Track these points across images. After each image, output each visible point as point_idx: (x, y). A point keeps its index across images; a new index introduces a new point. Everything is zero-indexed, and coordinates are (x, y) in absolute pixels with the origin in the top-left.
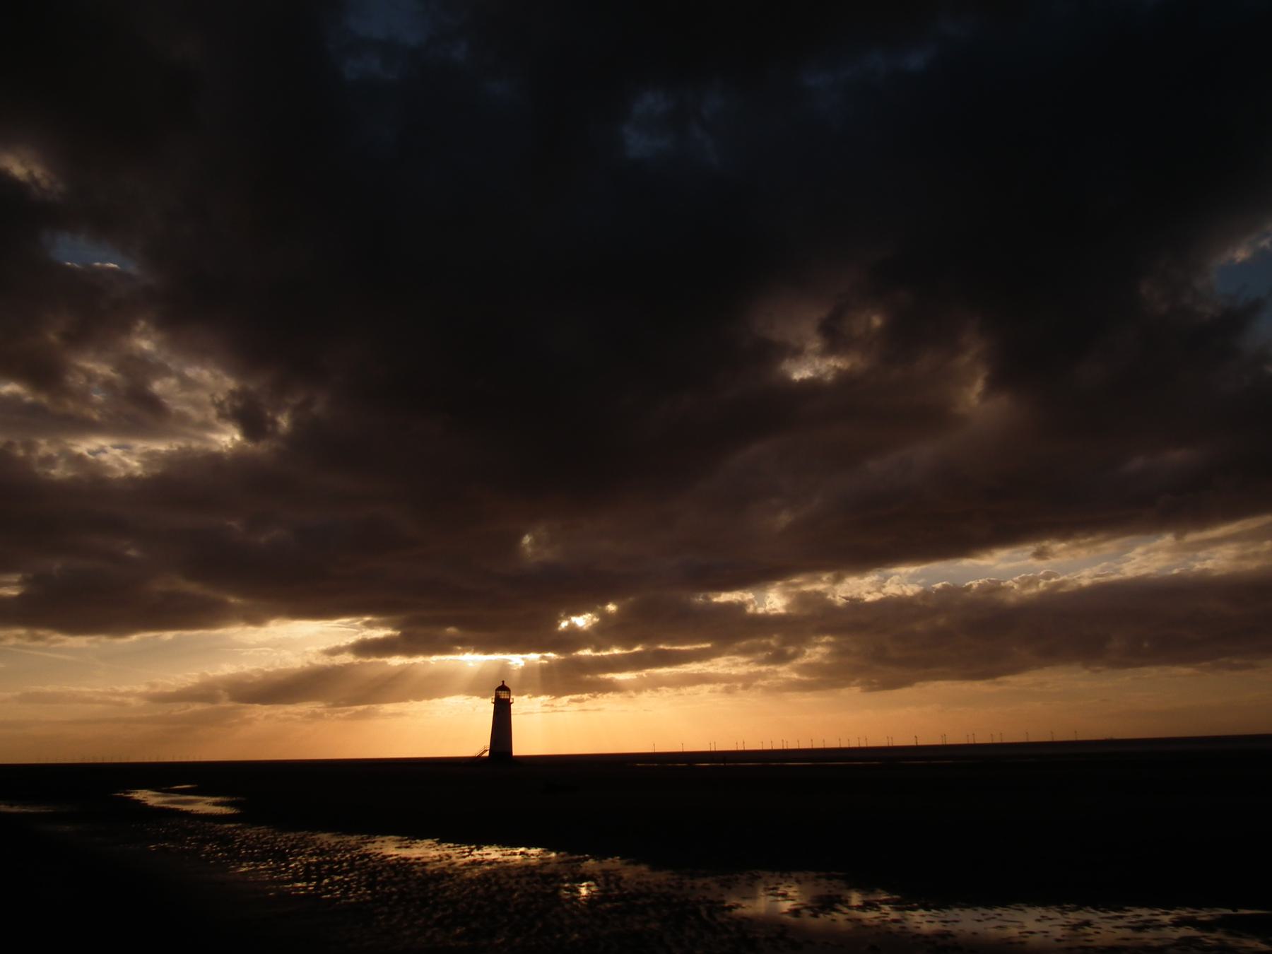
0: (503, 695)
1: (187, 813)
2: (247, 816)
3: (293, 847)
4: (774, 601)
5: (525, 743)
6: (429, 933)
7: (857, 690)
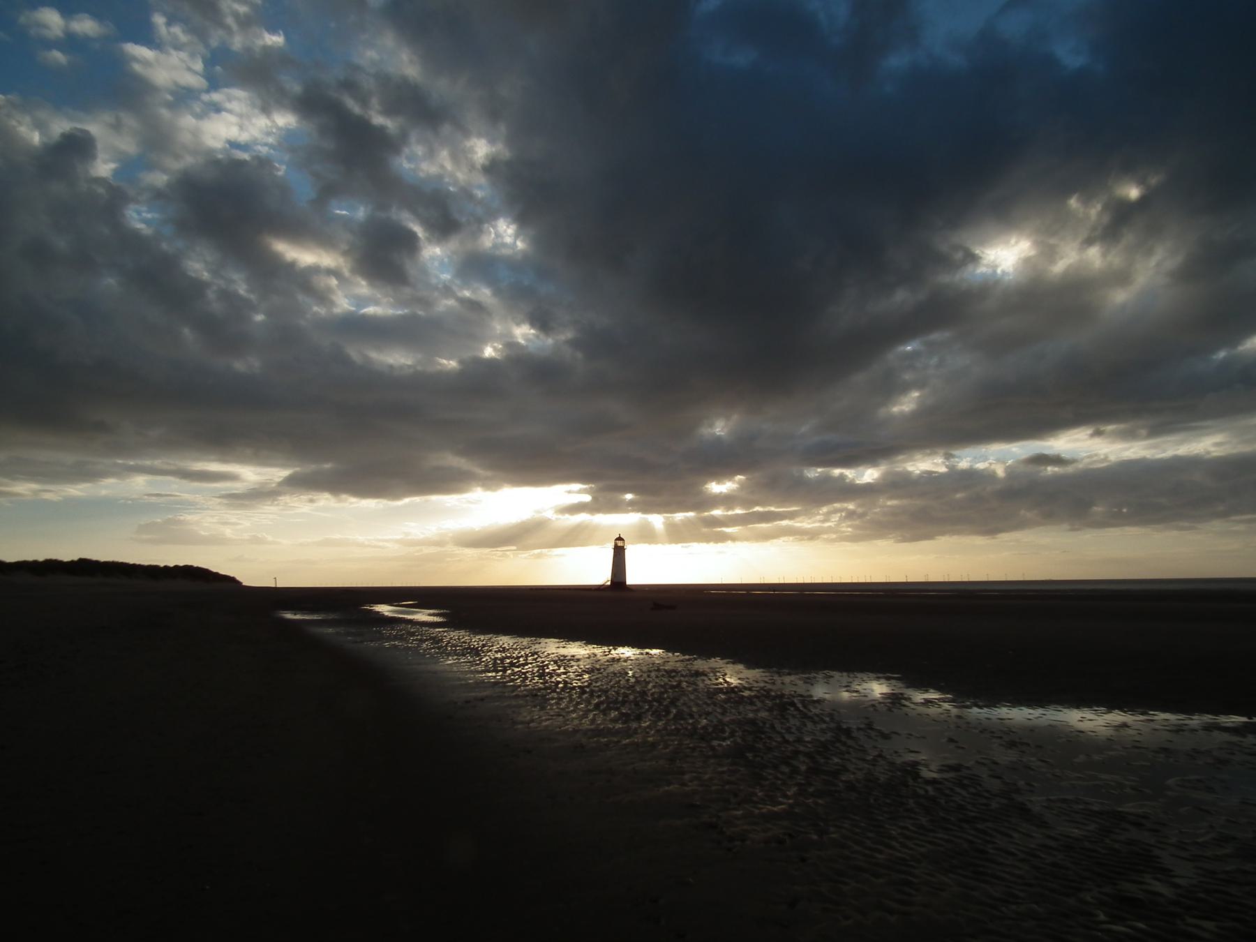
0: (620, 543)
1: (411, 621)
2: (453, 622)
3: (484, 646)
4: (869, 475)
5: (634, 577)
6: (591, 716)
7: (891, 542)
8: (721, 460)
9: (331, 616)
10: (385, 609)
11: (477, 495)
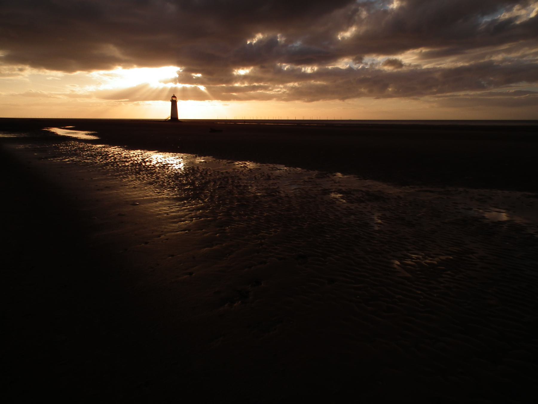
0: (174, 99)
5: (182, 115)
8: (248, 57)
9: (23, 135)
10: (60, 132)
11: (118, 70)
